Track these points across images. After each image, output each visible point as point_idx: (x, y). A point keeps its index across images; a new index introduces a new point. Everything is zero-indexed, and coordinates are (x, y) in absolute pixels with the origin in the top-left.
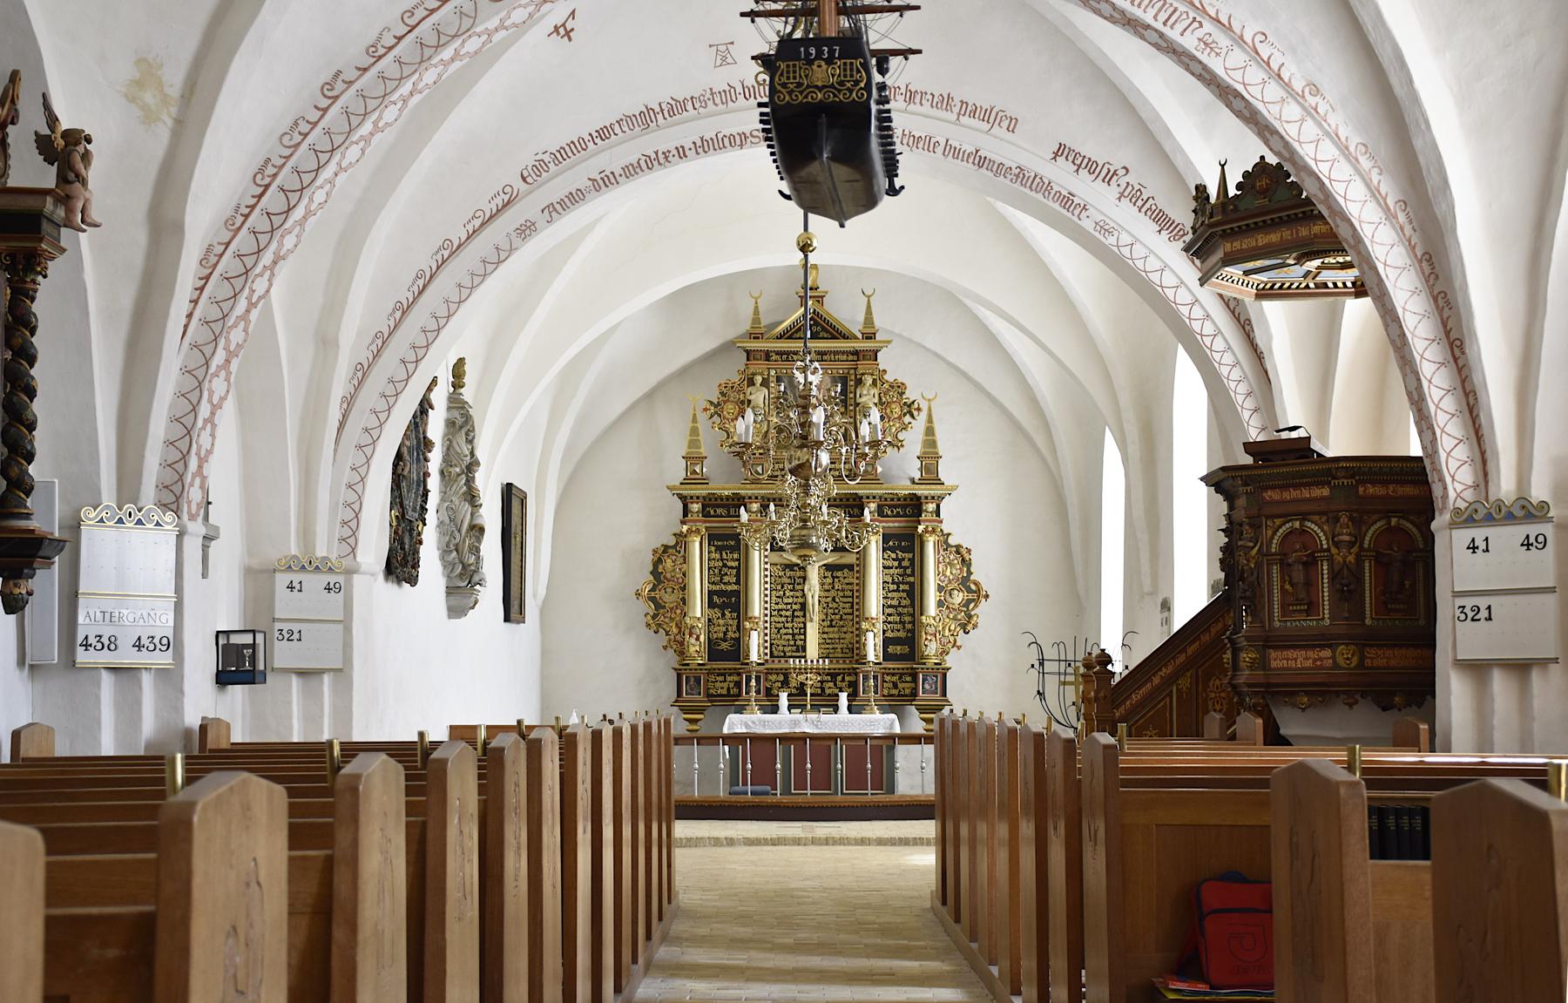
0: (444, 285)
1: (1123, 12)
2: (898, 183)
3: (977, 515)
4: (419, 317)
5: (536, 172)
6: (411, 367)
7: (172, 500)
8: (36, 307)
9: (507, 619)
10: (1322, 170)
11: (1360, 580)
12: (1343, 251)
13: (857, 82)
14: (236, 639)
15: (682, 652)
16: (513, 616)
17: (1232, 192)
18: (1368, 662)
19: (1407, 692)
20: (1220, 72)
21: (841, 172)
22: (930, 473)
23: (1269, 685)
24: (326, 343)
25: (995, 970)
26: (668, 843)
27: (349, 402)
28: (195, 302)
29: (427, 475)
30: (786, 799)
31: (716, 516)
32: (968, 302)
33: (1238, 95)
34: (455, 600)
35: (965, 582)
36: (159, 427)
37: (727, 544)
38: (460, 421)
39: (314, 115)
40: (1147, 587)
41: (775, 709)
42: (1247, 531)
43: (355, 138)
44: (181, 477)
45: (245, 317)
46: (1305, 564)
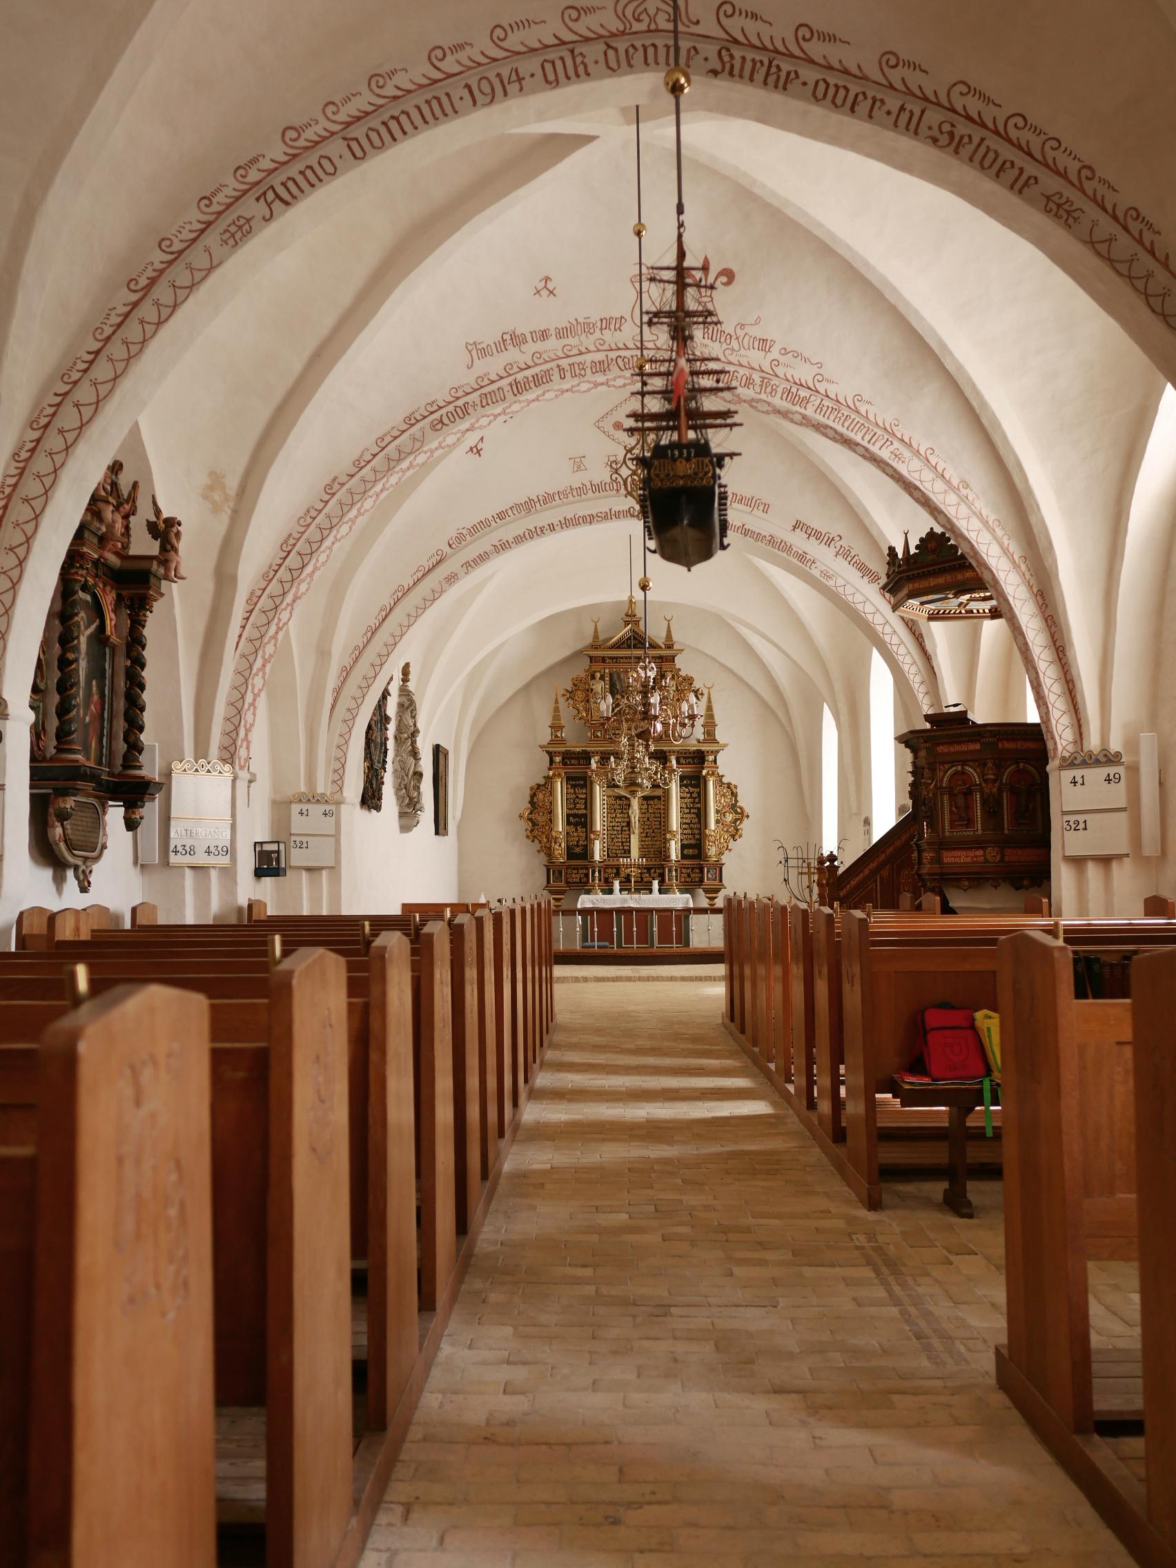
0: (398, 615)
1: (841, 435)
2: (726, 541)
3: (739, 763)
4: (383, 636)
5: (457, 542)
6: (377, 668)
7: (229, 755)
8: (146, 632)
9: (437, 833)
10: (972, 536)
11: (1000, 804)
12: (986, 589)
13: (706, 473)
14: (267, 847)
15: (550, 854)
16: (441, 831)
17: (913, 551)
18: (1006, 859)
19: (1031, 877)
20: (905, 473)
21: (692, 534)
22: (710, 736)
23: (942, 874)
24: (323, 654)
25: (772, 1066)
26: (550, 980)
27: (338, 691)
28: (243, 627)
29: (386, 739)
30: (620, 951)
31: (573, 765)
32: (734, 624)
33: (917, 488)
34: (405, 821)
35: (734, 807)
36: (220, 709)
37: (580, 783)
38: (407, 704)
39: (320, 506)
40: (854, 810)
41: (611, 892)
42: (927, 773)
43: (346, 519)
44: (234, 742)
45: (275, 637)
46: (965, 794)
